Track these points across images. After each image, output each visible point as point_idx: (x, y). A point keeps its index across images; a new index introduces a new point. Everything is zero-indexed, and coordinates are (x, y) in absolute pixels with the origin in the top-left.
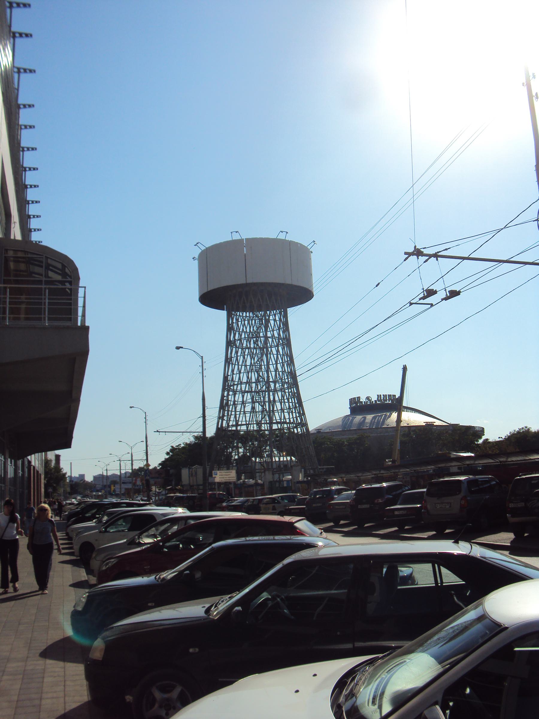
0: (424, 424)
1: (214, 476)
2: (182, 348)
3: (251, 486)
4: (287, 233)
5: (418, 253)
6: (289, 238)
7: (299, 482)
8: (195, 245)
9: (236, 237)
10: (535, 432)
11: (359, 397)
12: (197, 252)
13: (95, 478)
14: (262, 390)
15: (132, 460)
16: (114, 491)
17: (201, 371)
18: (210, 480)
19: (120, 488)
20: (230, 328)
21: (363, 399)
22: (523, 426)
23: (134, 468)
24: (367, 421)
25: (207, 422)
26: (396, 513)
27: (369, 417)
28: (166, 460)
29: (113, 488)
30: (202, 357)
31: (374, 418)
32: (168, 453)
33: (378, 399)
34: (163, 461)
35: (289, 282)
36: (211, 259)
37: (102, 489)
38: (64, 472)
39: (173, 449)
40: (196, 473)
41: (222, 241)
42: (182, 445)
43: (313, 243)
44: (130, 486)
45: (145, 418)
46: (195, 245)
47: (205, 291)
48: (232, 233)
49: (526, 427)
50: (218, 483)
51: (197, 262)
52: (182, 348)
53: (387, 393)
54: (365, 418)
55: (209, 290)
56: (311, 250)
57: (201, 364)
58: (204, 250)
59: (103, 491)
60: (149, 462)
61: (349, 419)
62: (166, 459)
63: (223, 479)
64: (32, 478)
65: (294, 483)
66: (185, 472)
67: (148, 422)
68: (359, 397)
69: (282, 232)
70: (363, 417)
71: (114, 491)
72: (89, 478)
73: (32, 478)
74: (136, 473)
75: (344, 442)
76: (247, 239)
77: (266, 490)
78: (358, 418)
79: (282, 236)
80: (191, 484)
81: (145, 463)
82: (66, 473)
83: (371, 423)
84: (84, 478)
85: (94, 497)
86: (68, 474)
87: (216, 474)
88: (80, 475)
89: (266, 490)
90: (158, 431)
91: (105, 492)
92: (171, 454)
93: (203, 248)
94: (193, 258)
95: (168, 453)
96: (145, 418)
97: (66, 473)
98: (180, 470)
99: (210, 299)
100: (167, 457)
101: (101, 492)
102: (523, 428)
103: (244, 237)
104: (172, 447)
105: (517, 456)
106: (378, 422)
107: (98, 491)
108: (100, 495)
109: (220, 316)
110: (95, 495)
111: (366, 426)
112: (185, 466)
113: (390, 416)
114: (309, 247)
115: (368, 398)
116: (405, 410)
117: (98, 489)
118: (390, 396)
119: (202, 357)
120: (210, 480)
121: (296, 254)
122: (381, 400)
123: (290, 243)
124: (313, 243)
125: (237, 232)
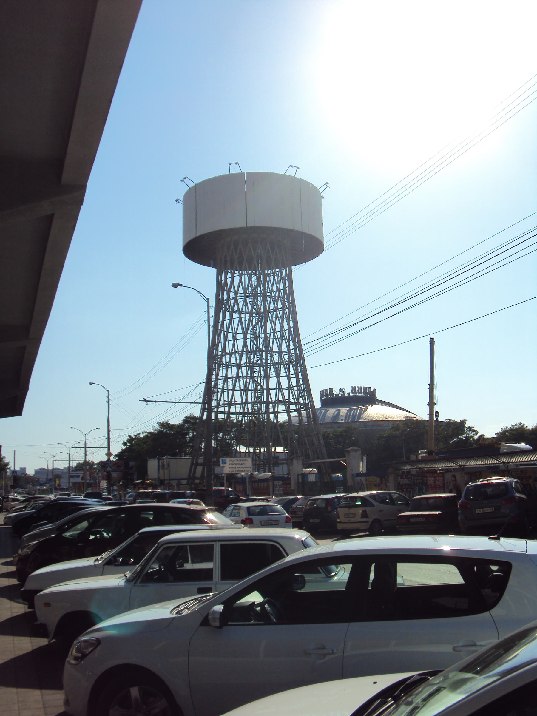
0: (404, 419)
1: (222, 465)
2: (181, 285)
3: (266, 480)
4: (298, 168)
5: (145, 400)
6: (299, 176)
7: (359, 475)
8: (182, 181)
9: (235, 170)
10: (532, 429)
11: (331, 389)
12: (181, 191)
13: (37, 472)
14: (259, 364)
15: (85, 448)
16: (59, 485)
17: (206, 319)
18: (217, 470)
19: (69, 482)
20: (221, 287)
21: (336, 392)
22: (517, 423)
23: (87, 460)
24: (341, 414)
25: (111, 440)
26: (412, 520)
27: (344, 411)
28: (123, 451)
29: (57, 482)
30: (208, 299)
31: (349, 411)
32: (125, 444)
33: (352, 391)
34: (120, 452)
35: (298, 228)
36: (200, 198)
37: (46, 483)
38: (6, 461)
39: (131, 440)
40: (169, 465)
41: (217, 176)
42: (142, 436)
43: (325, 186)
44: (79, 480)
45: (108, 397)
46: (182, 181)
47: (193, 236)
48: (230, 164)
49: (520, 424)
50: (227, 475)
51: (180, 207)
52: (181, 285)
53: (362, 385)
54: (339, 411)
55: (198, 235)
56: (322, 195)
57: (206, 310)
58: (193, 187)
59: (48, 485)
60: (111, 451)
61: (321, 412)
62: (122, 450)
63: (234, 470)
64: (373, 706)
65: (353, 475)
66: (152, 465)
67: (110, 402)
68: (331, 389)
69: (292, 167)
70: (337, 410)
71: (59, 485)
72: (30, 472)
73: (373, 706)
74: (79, 467)
75: (329, 434)
76: (249, 174)
77: (293, 486)
78: (332, 411)
79: (291, 172)
80: (162, 478)
81: (68, 465)
82: (7, 464)
83: (346, 417)
84: (25, 471)
85: (38, 492)
86: (11, 466)
87: (225, 463)
88: (21, 469)
89: (293, 486)
90: (145, 400)
91: (50, 486)
92: (128, 444)
93: (191, 185)
94: (176, 201)
95: (125, 444)
96: (108, 397)
97: (7, 464)
98: (146, 462)
99: (197, 249)
100: (124, 447)
101: (45, 486)
102: (516, 425)
103: (245, 171)
104: (130, 436)
105: (486, 459)
106: (354, 416)
107: (41, 485)
108: (44, 490)
109: (205, 277)
110: (39, 490)
111: (342, 419)
112: (154, 457)
113: (366, 410)
114: (321, 190)
115: (341, 390)
116: (380, 404)
117: (42, 482)
118: (365, 388)
119: (208, 299)
120: (217, 470)
121: (306, 196)
122: (355, 392)
123: (301, 182)
124: (325, 186)
125: (236, 164)
